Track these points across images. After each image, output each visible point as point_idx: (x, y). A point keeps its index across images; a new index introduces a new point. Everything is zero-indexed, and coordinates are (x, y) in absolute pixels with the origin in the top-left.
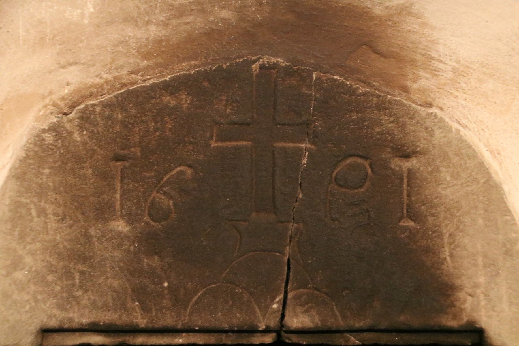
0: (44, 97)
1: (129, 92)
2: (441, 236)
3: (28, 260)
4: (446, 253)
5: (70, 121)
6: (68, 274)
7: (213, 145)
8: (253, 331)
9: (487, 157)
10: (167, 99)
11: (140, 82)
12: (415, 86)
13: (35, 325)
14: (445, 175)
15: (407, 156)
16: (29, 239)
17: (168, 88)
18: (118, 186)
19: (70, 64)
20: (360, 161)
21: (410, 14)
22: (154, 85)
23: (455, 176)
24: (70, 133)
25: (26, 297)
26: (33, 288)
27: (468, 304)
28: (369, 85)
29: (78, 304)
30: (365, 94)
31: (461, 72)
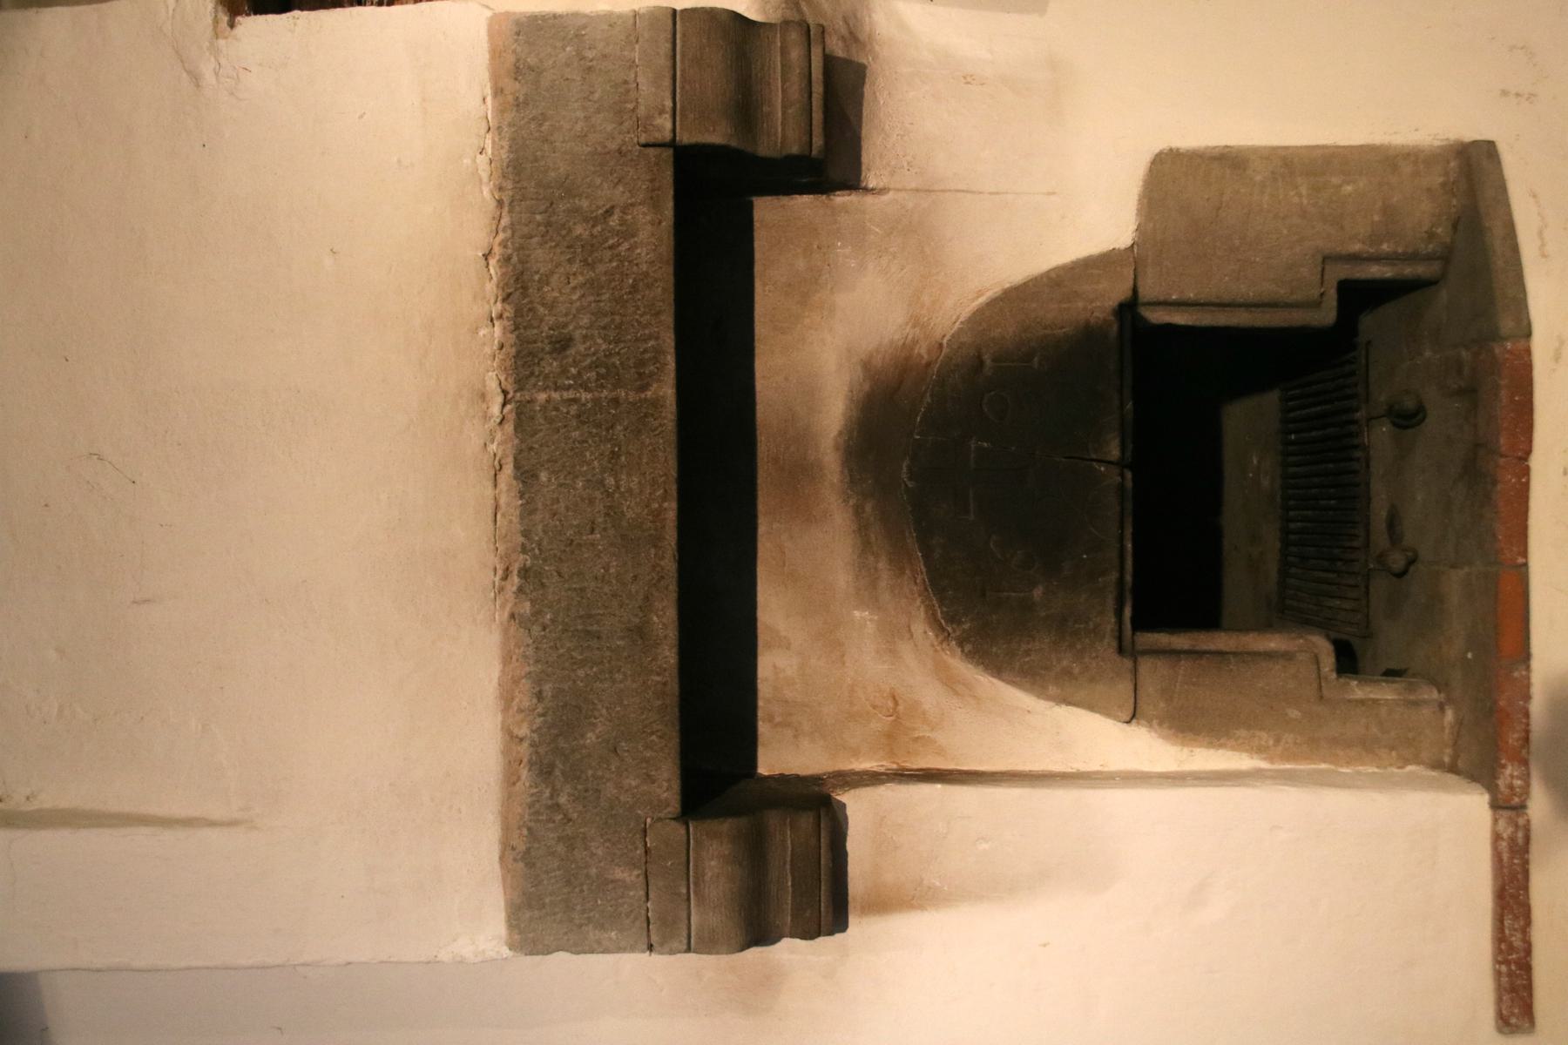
3: (1065, 663)
4: (1059, 332)
7: (972, 517)
9: (982, 300)
13: (1116, 657)
14: (996, 333)
15: (981, 363)
17: (927, 557)
31: (915, 322)
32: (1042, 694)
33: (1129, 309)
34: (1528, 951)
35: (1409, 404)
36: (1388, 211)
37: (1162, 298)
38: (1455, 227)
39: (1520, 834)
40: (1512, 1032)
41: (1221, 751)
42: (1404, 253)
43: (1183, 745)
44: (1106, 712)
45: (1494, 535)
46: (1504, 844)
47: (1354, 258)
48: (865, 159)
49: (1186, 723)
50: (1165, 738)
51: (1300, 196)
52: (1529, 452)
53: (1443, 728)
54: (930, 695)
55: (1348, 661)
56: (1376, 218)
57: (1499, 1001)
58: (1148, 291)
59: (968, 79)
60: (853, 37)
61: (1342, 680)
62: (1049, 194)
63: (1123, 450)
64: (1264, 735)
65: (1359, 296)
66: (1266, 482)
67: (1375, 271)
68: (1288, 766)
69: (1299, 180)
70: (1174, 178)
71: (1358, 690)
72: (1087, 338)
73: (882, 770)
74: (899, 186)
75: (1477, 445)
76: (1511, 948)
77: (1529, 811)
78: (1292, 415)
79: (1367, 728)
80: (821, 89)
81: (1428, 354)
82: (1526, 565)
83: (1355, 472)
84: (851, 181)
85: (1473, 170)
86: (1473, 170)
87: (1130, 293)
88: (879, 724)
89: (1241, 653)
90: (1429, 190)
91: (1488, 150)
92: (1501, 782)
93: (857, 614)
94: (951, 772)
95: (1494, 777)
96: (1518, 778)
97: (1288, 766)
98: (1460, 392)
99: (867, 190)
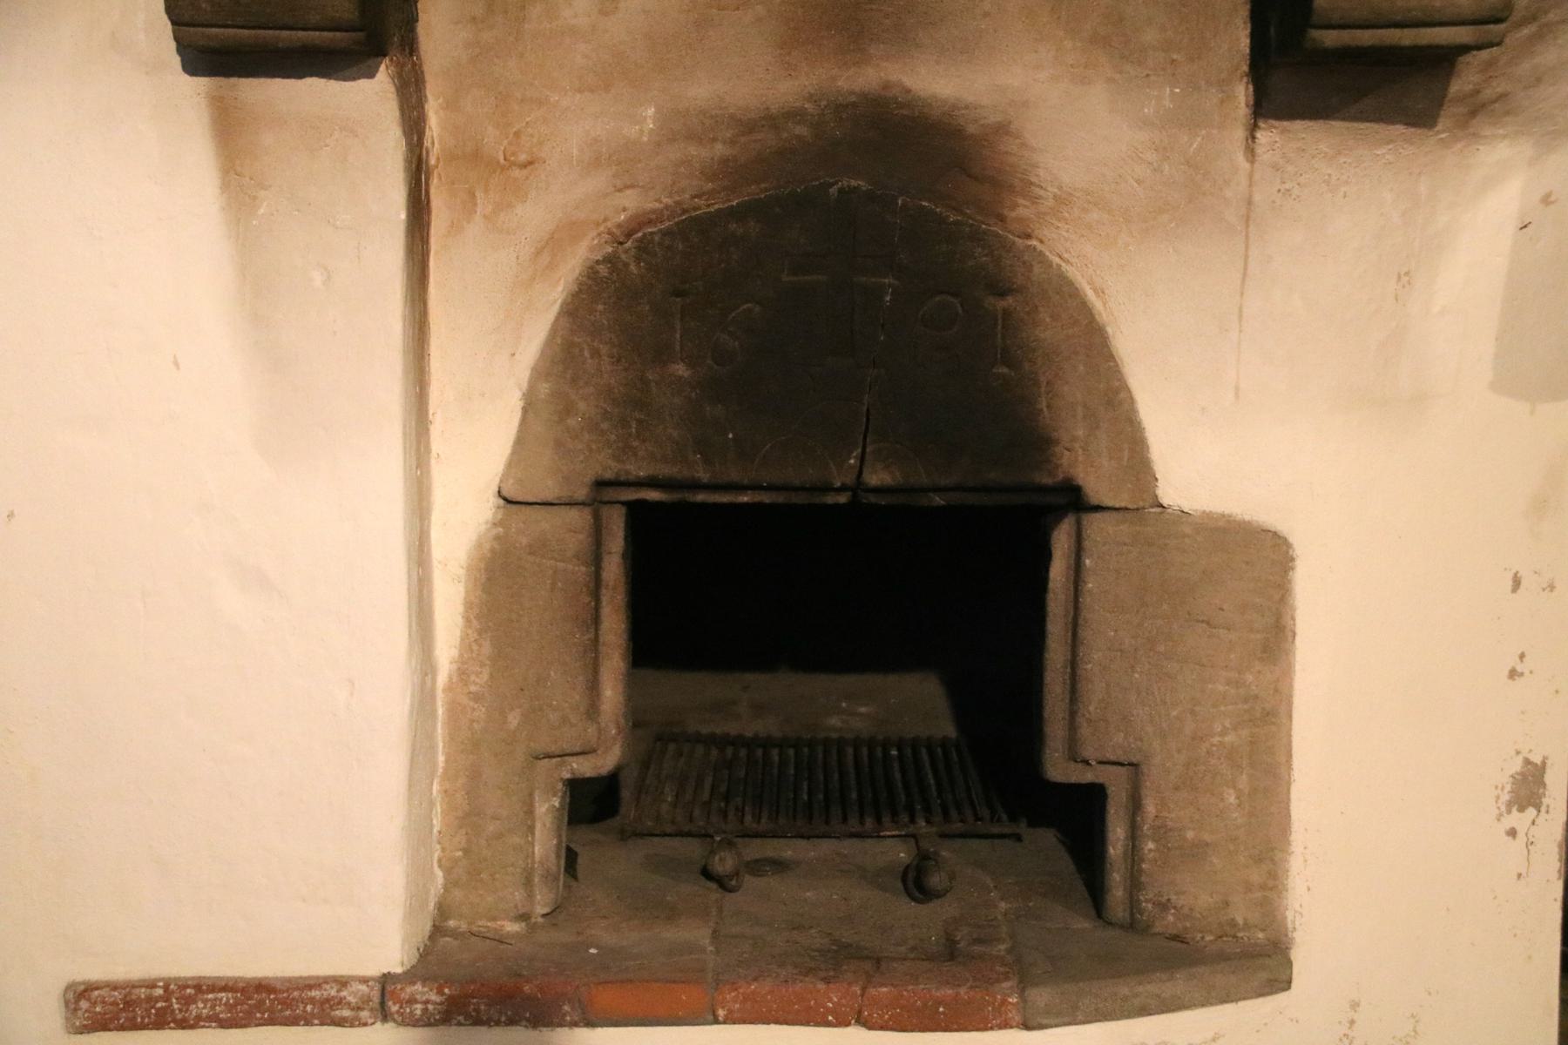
0: (598, 224)
1: (691, 219)
2: (1037, 383)
3: (582, 406)
4: (1043, 404)
5: (626, 252)
6: (623, 422)
7: (785, 278)
8: (828, 489)
9: (1090, 294)
10: (733, 226)
11: (705, 207)
12: (1013, 214)
13: (589, 477)
14: (1044, 315)
15: (1002, 294)
16: (581, 383)
17: (731, 213)
18: (678, 325)
19: (627, 187)
20: (952, 299)
21: (1007, 133)
22: (719, 211)
23: (1055, 317)
24: (626, 265)
25: (580, 447)
26: (587, 436)
27: (1065, 460)
28: (961, 213)
29: (635, 455)
30: (956, 223)
31: (1063, 200)
32: (538, 373)
33: (1073, 500)
34: (183, 1024)
35: (935, 880)
36: (1198, 852)
37: (1087, 544)
38: (1175, 938)
39: (346, 1013)
40: (67, 1003)
41: (460, 621)
42: (1141, 871)
43: (469, 569)
44: (511, 464)
45: (755, 979)
46: (333, 993)
47: (1136, 804)
48: (1298, 125)
49: (498, 572)
50: (479, 545)
51: (1223, 733)
52: (870, 1026)
53: (494, 919)
54: (536, 214)
55: (591, 803)
56: (1190, 835)
57: (114, 986)
58: (1096, 525)
59: (1405, 279)
60: (1477, 109)
61: (560, 786)
62: (1237, 389)
63: (877, 490)
64: (485, 677)
65: (1078, 818)
66: (834, 721)
67: (1117, 833)
68: (440, 711)
69: (1245, 733)
70: (1253, 561)
71: (548, 806)
72: (1032, 440)
73: (427, 143)
74: (1257, 176)
75: (878, 961)
76: (187, 1001)
77: (378, 1025)
78: (924, 751)
79: (495, 818)
80: (1406, 42)
81: (1003, 905)
82: (716, 1021)
83: (845, 820)
84: (1270, 104)
85: (1253, 960)
86: (1253, 960)
87: (1094, 501)
88: (493, 140)
89: (596, 651)
90: (1227, 904)
91: (1279, 982)
92: (418, 987)
93: (651, 111)
94: (425, 241)
95: (425, 981)
96: (425, 1010)
97: (440, 711)
98: (951, 942)
99: (1253, 129)
